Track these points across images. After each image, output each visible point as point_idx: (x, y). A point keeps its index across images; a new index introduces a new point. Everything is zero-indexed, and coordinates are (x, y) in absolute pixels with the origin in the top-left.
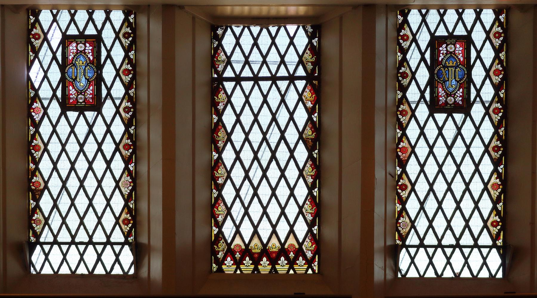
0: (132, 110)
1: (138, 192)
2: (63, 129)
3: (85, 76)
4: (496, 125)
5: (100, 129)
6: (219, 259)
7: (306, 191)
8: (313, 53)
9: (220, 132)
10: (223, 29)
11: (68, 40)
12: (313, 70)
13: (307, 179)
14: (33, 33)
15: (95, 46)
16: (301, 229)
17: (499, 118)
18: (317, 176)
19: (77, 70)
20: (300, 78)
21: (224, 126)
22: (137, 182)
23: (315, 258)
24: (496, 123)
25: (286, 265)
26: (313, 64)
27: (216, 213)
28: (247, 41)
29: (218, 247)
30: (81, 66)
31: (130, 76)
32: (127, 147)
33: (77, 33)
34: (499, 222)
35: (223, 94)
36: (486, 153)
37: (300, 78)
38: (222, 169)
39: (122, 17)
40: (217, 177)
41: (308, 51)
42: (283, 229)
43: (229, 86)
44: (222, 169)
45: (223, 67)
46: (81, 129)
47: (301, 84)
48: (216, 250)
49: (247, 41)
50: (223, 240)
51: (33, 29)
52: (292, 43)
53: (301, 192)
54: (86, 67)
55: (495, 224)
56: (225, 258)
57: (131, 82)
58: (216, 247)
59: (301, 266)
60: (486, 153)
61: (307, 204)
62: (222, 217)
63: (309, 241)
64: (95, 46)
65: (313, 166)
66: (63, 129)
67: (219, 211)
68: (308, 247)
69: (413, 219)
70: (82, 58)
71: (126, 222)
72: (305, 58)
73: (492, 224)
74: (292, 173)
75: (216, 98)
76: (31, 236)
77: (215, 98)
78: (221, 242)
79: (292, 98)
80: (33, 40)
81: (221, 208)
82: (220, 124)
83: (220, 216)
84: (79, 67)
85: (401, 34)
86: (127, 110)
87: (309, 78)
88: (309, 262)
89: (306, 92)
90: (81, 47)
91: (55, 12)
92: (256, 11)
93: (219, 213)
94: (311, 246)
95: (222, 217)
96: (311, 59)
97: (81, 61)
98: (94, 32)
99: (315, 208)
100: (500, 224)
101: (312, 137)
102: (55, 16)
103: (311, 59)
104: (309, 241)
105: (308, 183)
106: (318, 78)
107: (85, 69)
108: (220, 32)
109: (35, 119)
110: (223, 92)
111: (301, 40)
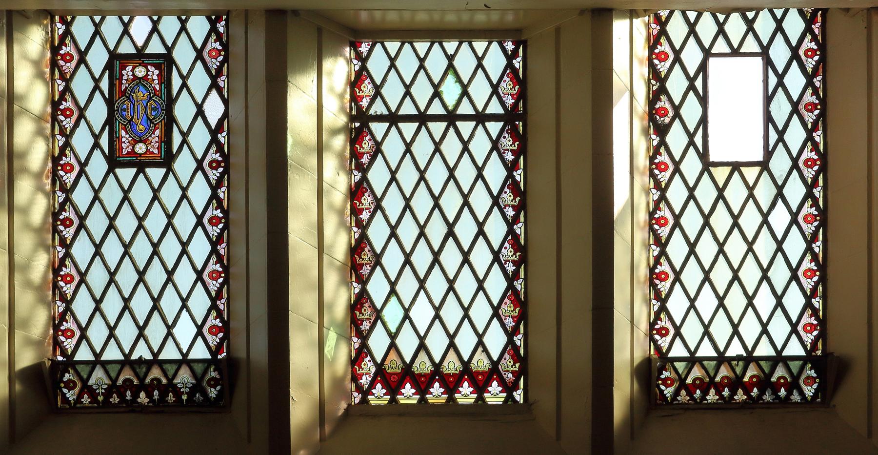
0: (223, 221)
1: (231, 341)
2: (111, 195)
3: (147, 115)
4: (810, 73)
5: (170, 194)
6: (362, 164)
7: (503, 339)
8: (515, 247)
9: (364, 85)
10: (368, 45)
11: (117, 157)
12: (515, 106)
13: (505, 322)
14: (62, 52)
15: (163, 81)
16: (496, 341)
17: (814, 229)
18: (522, 317)
19: (134, 105)
20: (495, 118)
21: (370, 353)
22: (230, 49)
23: (518, 52)
24: (810, 71)
25: (471, 393)
26: (516, 208)
27: (358, 372)
28: (407, 63)
29: (361, 258)
30: (141, 100)
31: (221, 170)
32: (214, 54)
33: (133, 51)
34: (815, 160)
35: (369, 83)
36: (795, 61)
37: (495, 118)
38: (368, 308)
39: (207, 26)
40: (359, 375)
41: (507, 356)
42: (466, 342)
43: (378, 129)
44: (368, 308)
45: (369, 101)
46: (141, 195)
47: (494, 128)
48: (358, 372)
49: (407, 63)
50: (368, 80)
51: (62, 158)
52: (481, 233)
53: (496, 229)
54: (149, 102)
55: (809, 274)
56: (372, 385)
57: (220, 237)
58: (357, 90)
59: (495, 395)
60: (795, 61)
61: (506, 248)
62: (368, 323)
63: (507, 81)
64: (163, 81)
65: (515, 247)
66: (111, 195)
67: (363, 369)
68: (508, 366)
69: (677, 103)
70: (142, 89)
71: (214, 221)
72: (501, 145)
73: (805, 274)
74: (481, 257)
75: (358, 203)
76: (57, 134)
77: (357, 148)
78: (367, 194)
79: (481, 146)
80: (62, 63)
81: (366, 199)
82: (365, 73)
83: (364, 100)
84: (138, 102)
85: (657, 51)
86: (214, 330)
87: (509, 117)
88: (509, 388)
89: (505, 81)
90: (140, 72)
91: (97, 19)
92: (422, 18)
93: (363, 94)
94: (513, 144)
95: (368, 323)
96: (512, 367)
97: (141, 94)
98: (162, 50)
99: (518, 143)
100: (819, 107)
101: (514, 369)
102: (97, 26)
103: (512, 90)
104: (508, 80)
105: (507, 105)
106: (523, 117)
107: (147, 104)
108: (364, 48)
109: (69, 398)
110: (369, 358)
111: (495, 61)
